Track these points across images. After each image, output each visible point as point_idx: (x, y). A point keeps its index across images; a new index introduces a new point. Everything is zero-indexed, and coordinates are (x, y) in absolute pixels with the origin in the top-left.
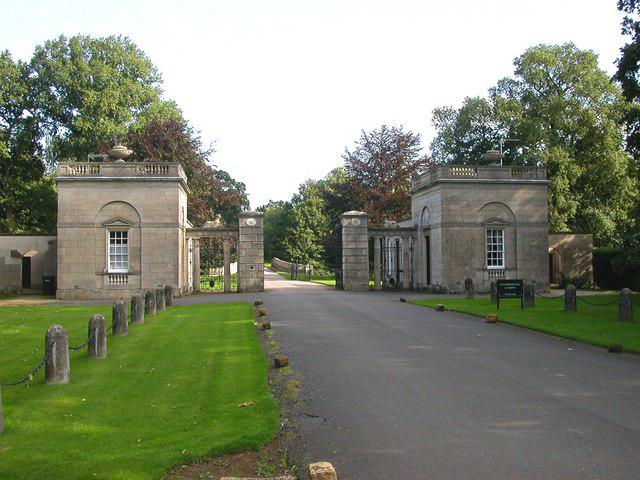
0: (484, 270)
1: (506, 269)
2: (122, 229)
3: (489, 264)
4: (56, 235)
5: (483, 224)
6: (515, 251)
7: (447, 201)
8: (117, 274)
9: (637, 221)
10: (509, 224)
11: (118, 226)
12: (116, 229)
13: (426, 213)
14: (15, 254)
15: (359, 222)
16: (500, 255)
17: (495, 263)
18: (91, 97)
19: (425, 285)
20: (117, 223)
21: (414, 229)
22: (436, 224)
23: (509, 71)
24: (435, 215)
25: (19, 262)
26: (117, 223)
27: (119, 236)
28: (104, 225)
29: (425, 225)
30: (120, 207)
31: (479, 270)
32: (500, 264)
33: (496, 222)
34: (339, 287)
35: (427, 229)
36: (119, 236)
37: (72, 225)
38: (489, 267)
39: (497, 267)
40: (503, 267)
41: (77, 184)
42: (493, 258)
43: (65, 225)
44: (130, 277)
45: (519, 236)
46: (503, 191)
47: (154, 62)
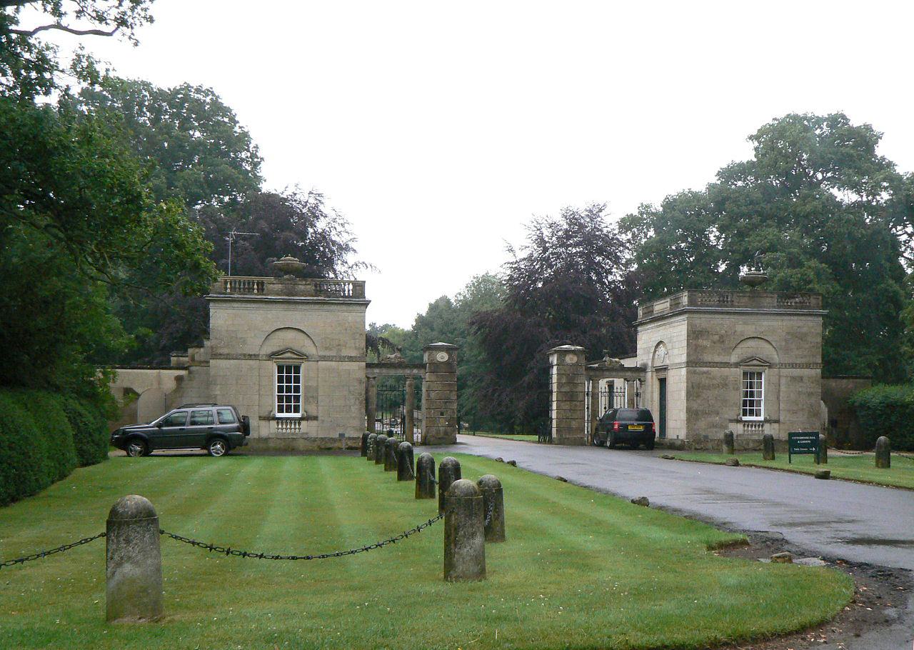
1: (766, 421)
3: (745, 414)
6: (778, 398)
9: (49, 192)
11: (289, 359)
13: (662, 350)
15: (575, 359)
16: (759, 403)
17: (289, 410)
20: (289, 355)
21: (643, 369)
23: (715, 180)
24: (676, 351)
26: (289, 355)
27: (289, 371)
28: (272, 356)
29: (658, 364)
30: (290, 335)
31: (731, 421)
32: (297, 410)
34: (129, 455)
36: (289, 371)
38: (745, 418)
39: (292, 415)
41: (235, 305)
42: (749, 405)
44: (303, 423)
47: (256, 138)
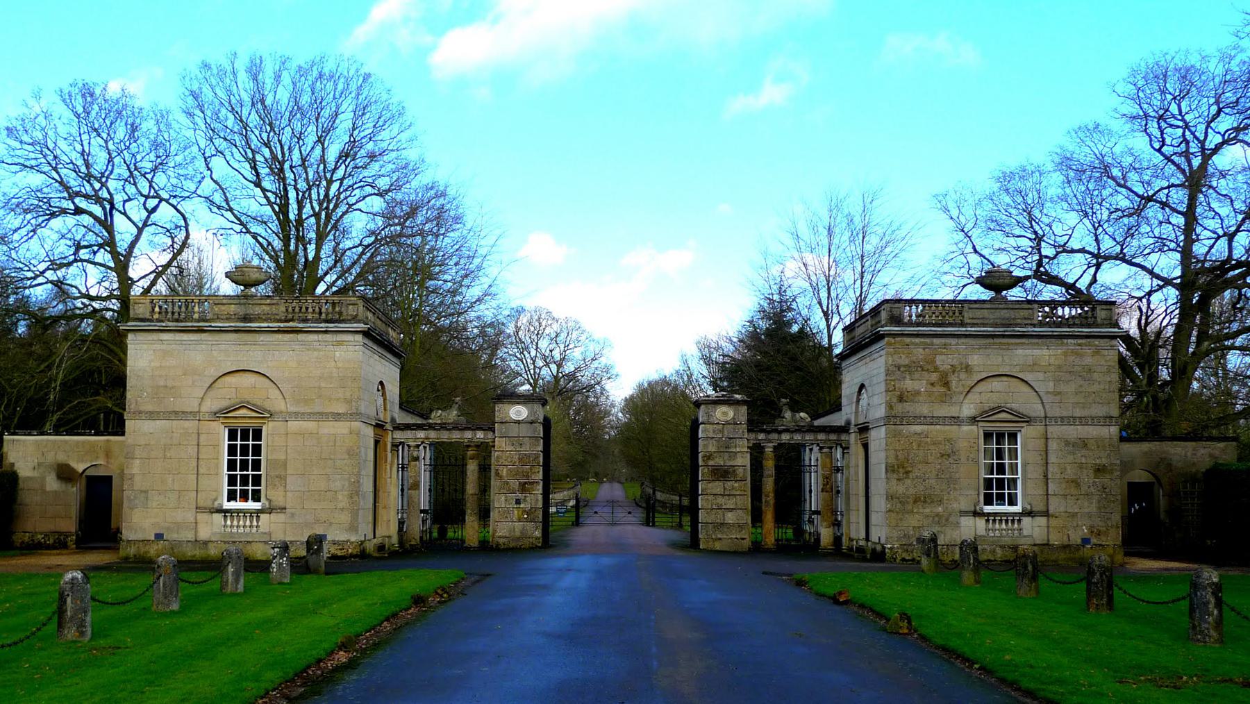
0: (977, 514)
1: (1027, 513)
2: (251, 424)
3: (989, 501)
4: (116, 425)
5: (973, 420)
7: (895, 371)
8: (996, 514)
10: (1029, 421)
11: (244, 419)
12: (240, 424)
13: (864, 395)
14: (65, 473)
15: (731, 414)
17: (244, 497)
18: (1161, 112)
19: (862, 543)
21: (844, 429)
22: (877, 420)
25: (75, 493)
27: (245, 436)
32: (1012, 502)
33: (1003, 416)
35: (864, 429)
37: (152, 416)
38: (988, 509)
39: (251, 505)
40: (1017, 509)
43: (139, 414)
45: (1053, 446)
46: (1019, 352)
